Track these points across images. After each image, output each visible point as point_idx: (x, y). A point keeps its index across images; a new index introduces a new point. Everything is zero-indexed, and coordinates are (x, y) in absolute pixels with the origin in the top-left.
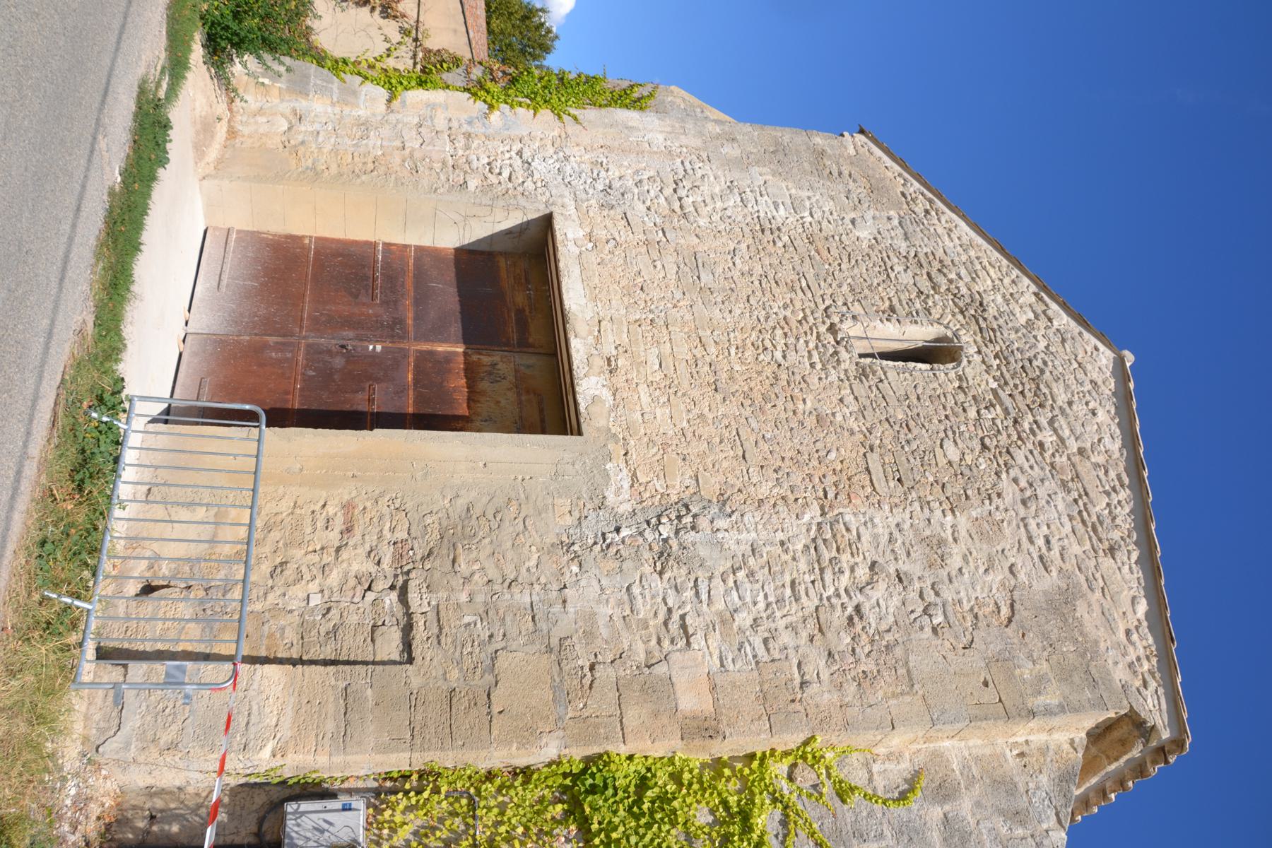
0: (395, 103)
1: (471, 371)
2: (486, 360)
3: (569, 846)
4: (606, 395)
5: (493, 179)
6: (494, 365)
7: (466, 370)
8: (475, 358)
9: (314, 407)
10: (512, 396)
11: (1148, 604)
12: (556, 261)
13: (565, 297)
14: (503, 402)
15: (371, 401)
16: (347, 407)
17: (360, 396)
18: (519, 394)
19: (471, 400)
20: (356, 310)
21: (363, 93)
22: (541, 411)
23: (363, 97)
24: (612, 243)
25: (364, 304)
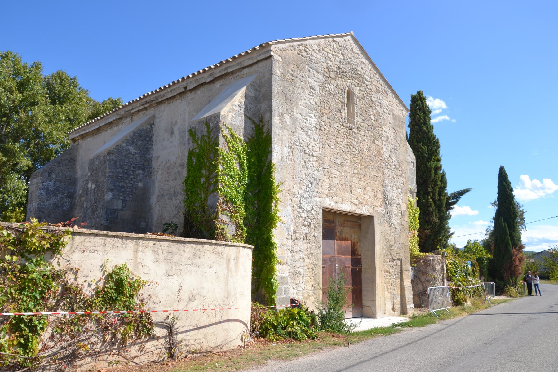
0: (284, 261)
1: (341, 239)
2: (338, 234)
3: (557, 265)
4: (367, 207)
5: (312, 226)
6: (339, 232)
7: (341, 240)
8: (337, 237)
9: (351, 282)
10: (345, 228)
11: (537, 179)
12: (337, 210)
13: (347, 211)
14: (347, 231)
15: (349, 267)
16: (351, 273)
17: (348, 270)
18: (345, 226)
19: (347, 240)
20: (328, 272)
21: (281, 275)
22: (349, 221)
23: (283, 275)
24: (329, 189)
25: (326, 270)
